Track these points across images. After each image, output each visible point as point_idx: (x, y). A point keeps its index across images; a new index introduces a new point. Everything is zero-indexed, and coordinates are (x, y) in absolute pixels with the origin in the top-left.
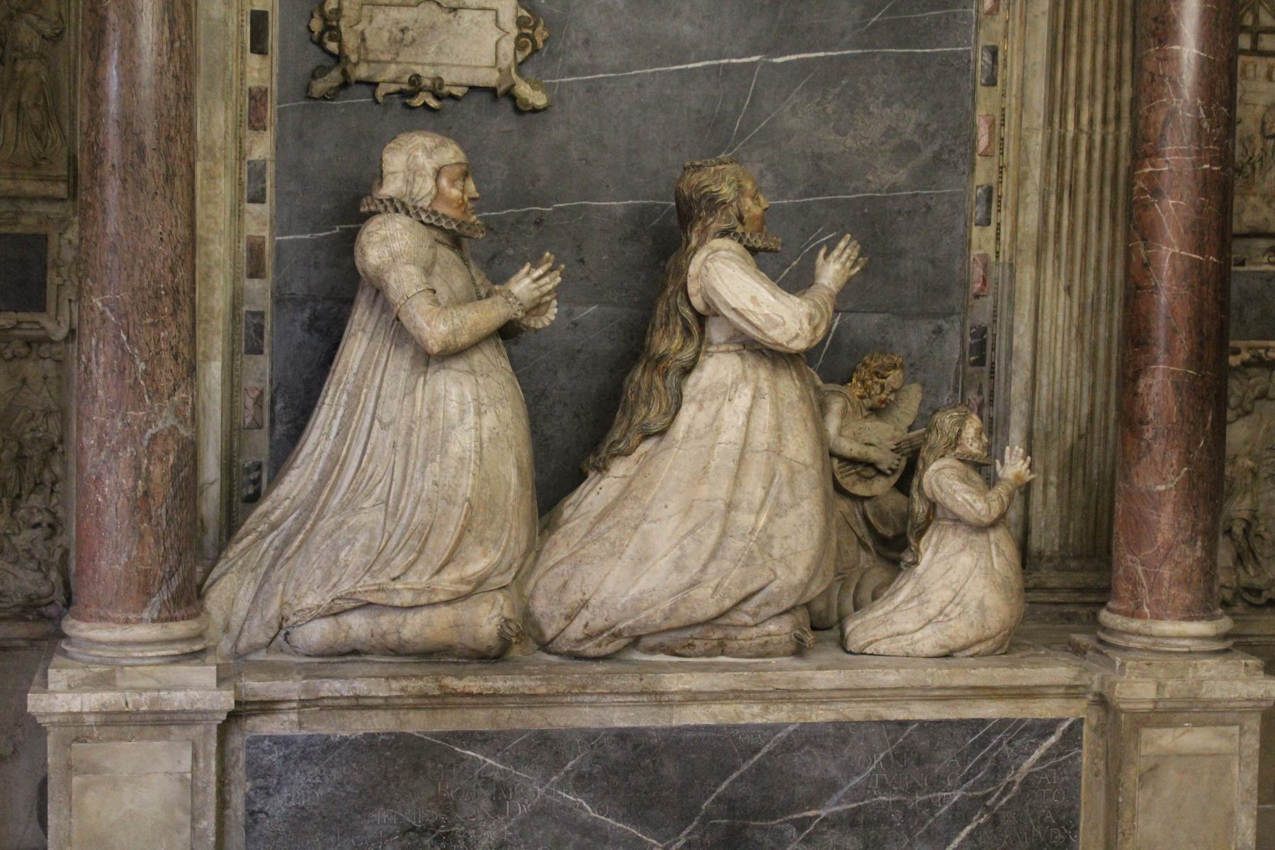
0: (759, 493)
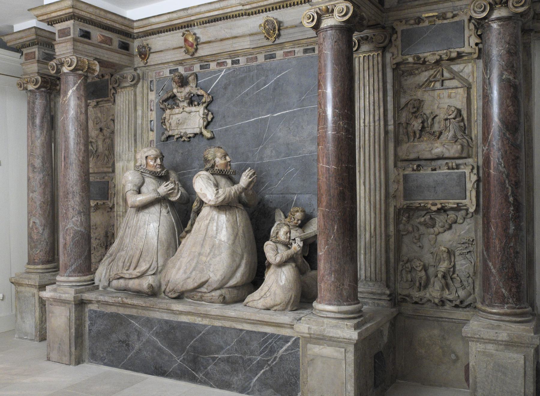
0: (208, 251)
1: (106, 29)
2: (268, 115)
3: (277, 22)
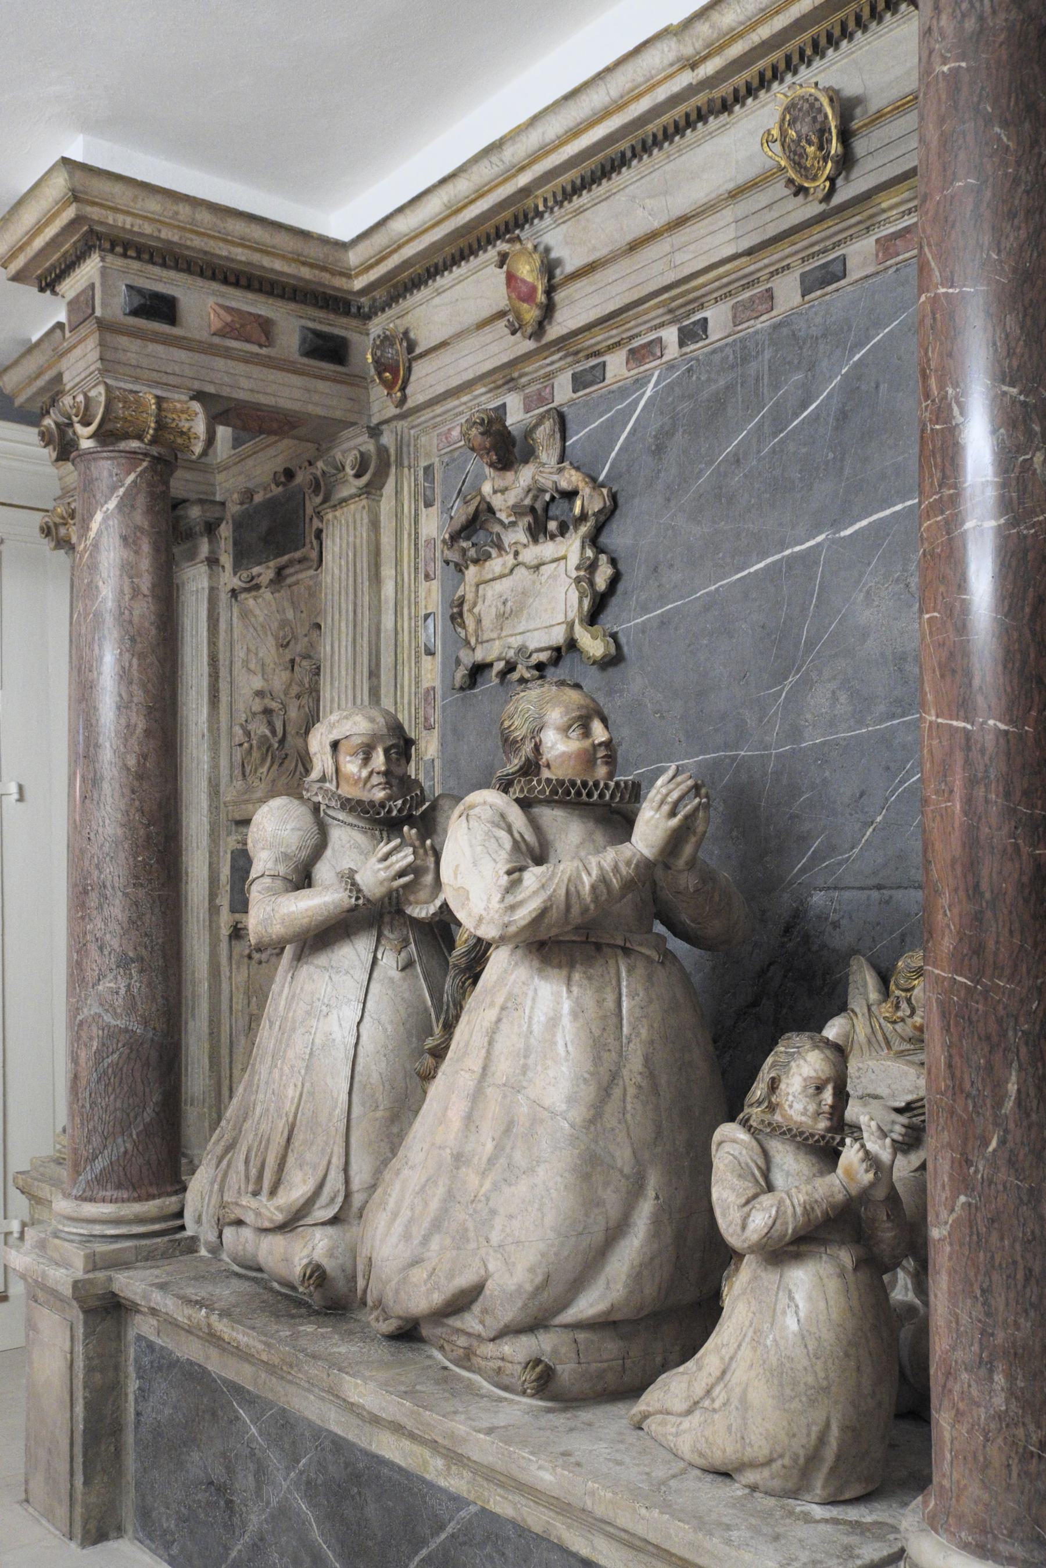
0: (490, 1146)
1: (237, 284)
2: (820, 538)
3: (831, 100)
